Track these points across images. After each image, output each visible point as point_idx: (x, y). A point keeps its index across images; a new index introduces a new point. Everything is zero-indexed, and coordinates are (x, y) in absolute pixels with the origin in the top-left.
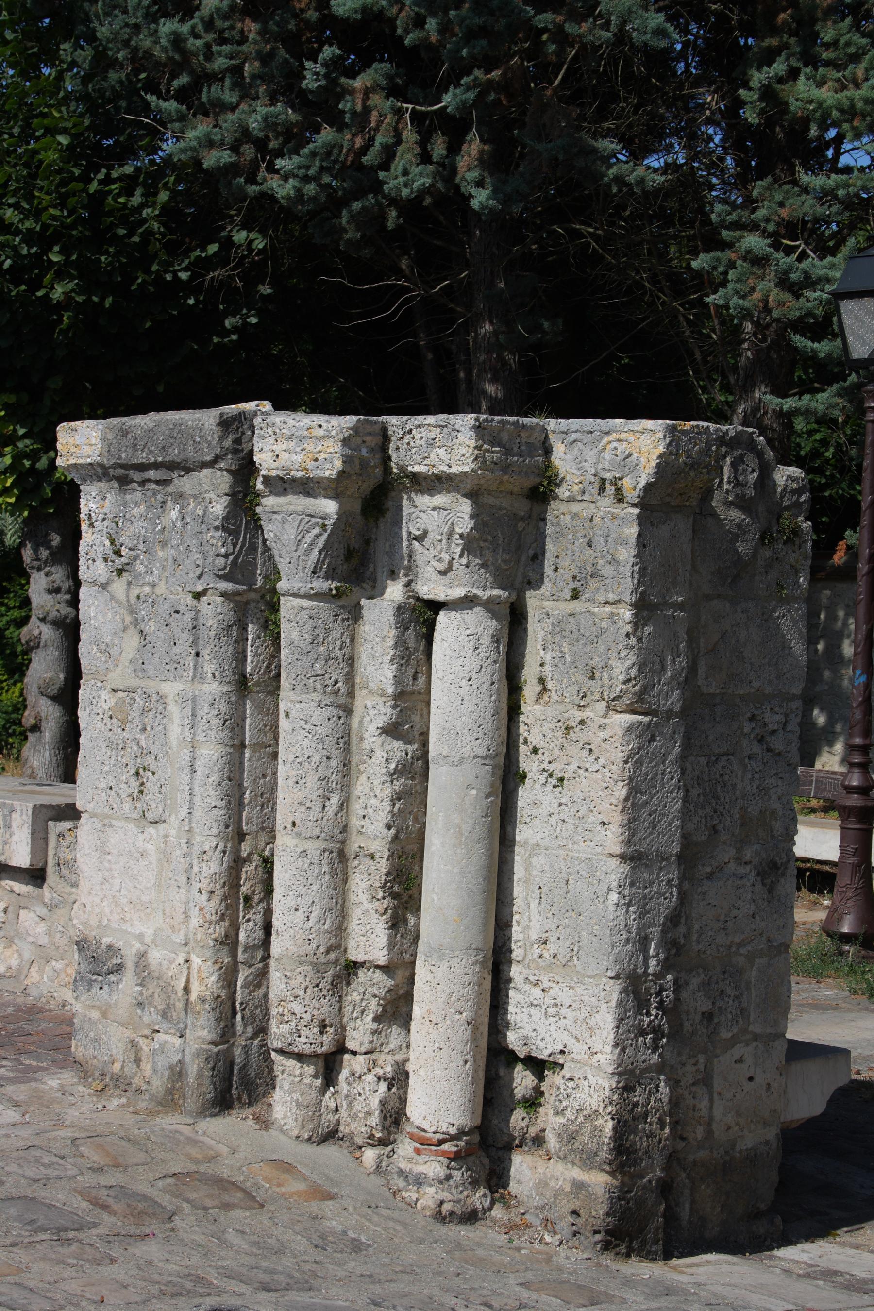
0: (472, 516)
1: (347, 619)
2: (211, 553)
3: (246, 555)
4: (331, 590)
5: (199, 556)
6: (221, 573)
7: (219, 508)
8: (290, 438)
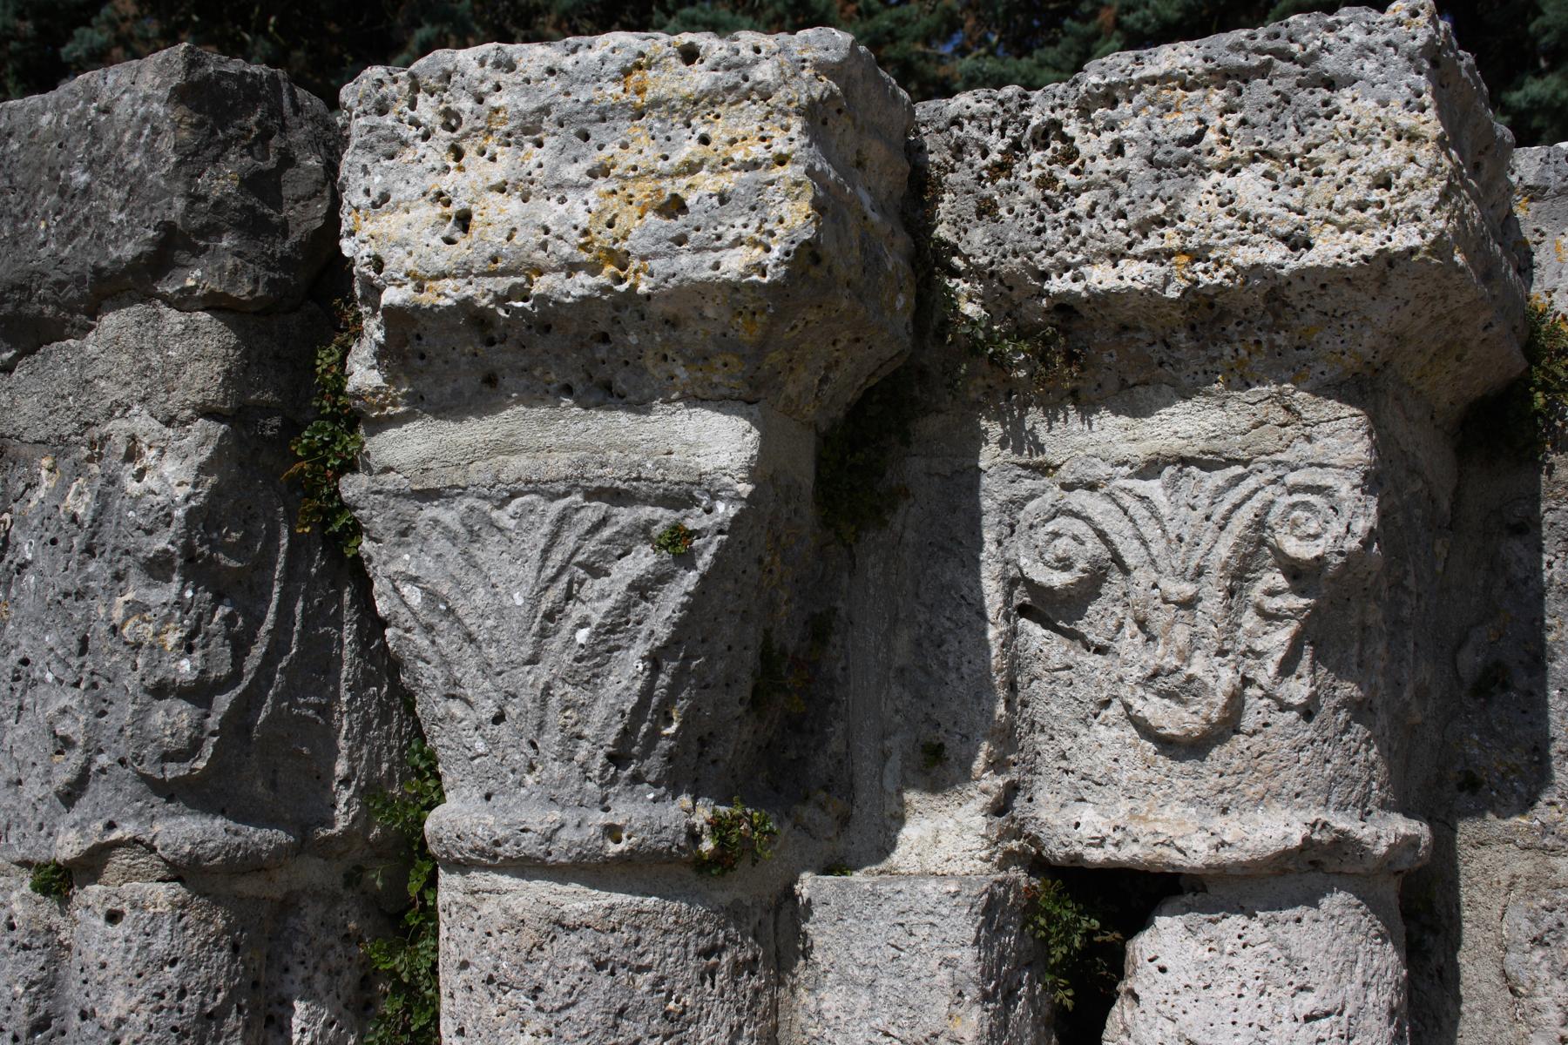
0: (1372, 482)
1: (751, 966)
2: (131, 681)
3: (290, 692)
4: (694, 836)
5: (70, 699)
6: (173, 771)
7: (172, 474)
8: (530, 129)
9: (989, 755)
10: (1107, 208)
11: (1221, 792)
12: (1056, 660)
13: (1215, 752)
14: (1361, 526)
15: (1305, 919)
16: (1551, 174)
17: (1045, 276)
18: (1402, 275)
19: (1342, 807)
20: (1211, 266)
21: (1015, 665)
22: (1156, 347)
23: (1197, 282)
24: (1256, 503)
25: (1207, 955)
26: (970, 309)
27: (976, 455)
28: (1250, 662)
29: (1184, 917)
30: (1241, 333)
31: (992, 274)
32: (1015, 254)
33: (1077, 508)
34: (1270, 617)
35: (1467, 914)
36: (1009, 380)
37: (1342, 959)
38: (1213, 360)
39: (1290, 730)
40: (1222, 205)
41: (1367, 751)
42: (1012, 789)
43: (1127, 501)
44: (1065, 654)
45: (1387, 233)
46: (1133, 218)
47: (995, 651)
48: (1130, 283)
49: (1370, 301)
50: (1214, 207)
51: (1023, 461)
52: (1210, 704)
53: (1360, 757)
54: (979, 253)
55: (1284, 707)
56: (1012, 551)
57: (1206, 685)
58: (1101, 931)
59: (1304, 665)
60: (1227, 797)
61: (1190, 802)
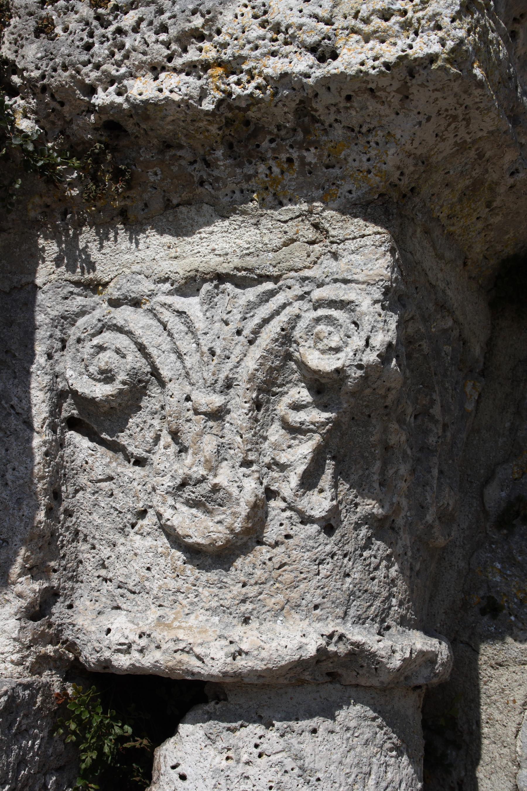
0: (393, 298)
9: (26, 560)
10: (151, 23)
11: (244, 601)
12: (99, 472)
13: (239, 563)
14: (380, 340)
15: (321, 731)
17: (91, 90)
18: (422, 85)
19: (360, 620)
20: (244, 77)
21: (60, 475)
22: (196, 166)
23: (230, 94)
24: (283, 318)
25: (224, 763)
26: (25, 125)
27: (34, 272)
28: (275, 474)
29: (205, 725)
30: (274, 150)
31: (44, 88)
32: (65, 68)
33: (120, 322)
34: (295, 430)
35: (485, 730)
36: (63, 199)
37: (355, 771)
38: (248, 178)
39: (311, 543)
40: (255, 17)
41: (388, 568)
42: (50, 596)
43: (167, 316)
44: (107, 465)
45: (409, 41)
46: (173, 31)
47: (38, 459)
48: (166, 93)
49: (393, 116)
50: (248, 20)
51: (75, 278)
52: (234, 514)
53: (381, 573)
54: (31, 66)
55: (306, 520)
56: (62, 365)
57: (230, 495)
58: (132, 738)
59: (326, 480)
60: (249, 606)
61: (213, 611)
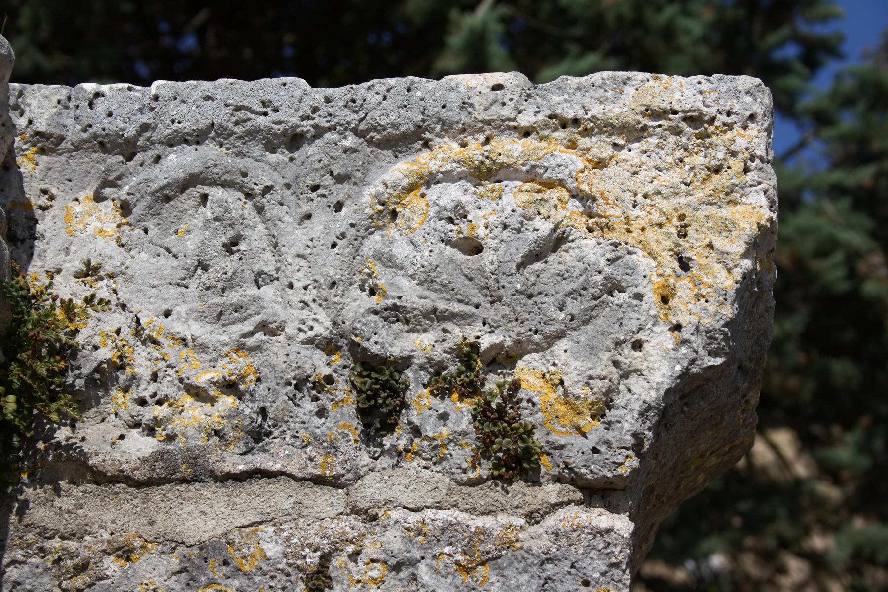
16: (69, 122)
